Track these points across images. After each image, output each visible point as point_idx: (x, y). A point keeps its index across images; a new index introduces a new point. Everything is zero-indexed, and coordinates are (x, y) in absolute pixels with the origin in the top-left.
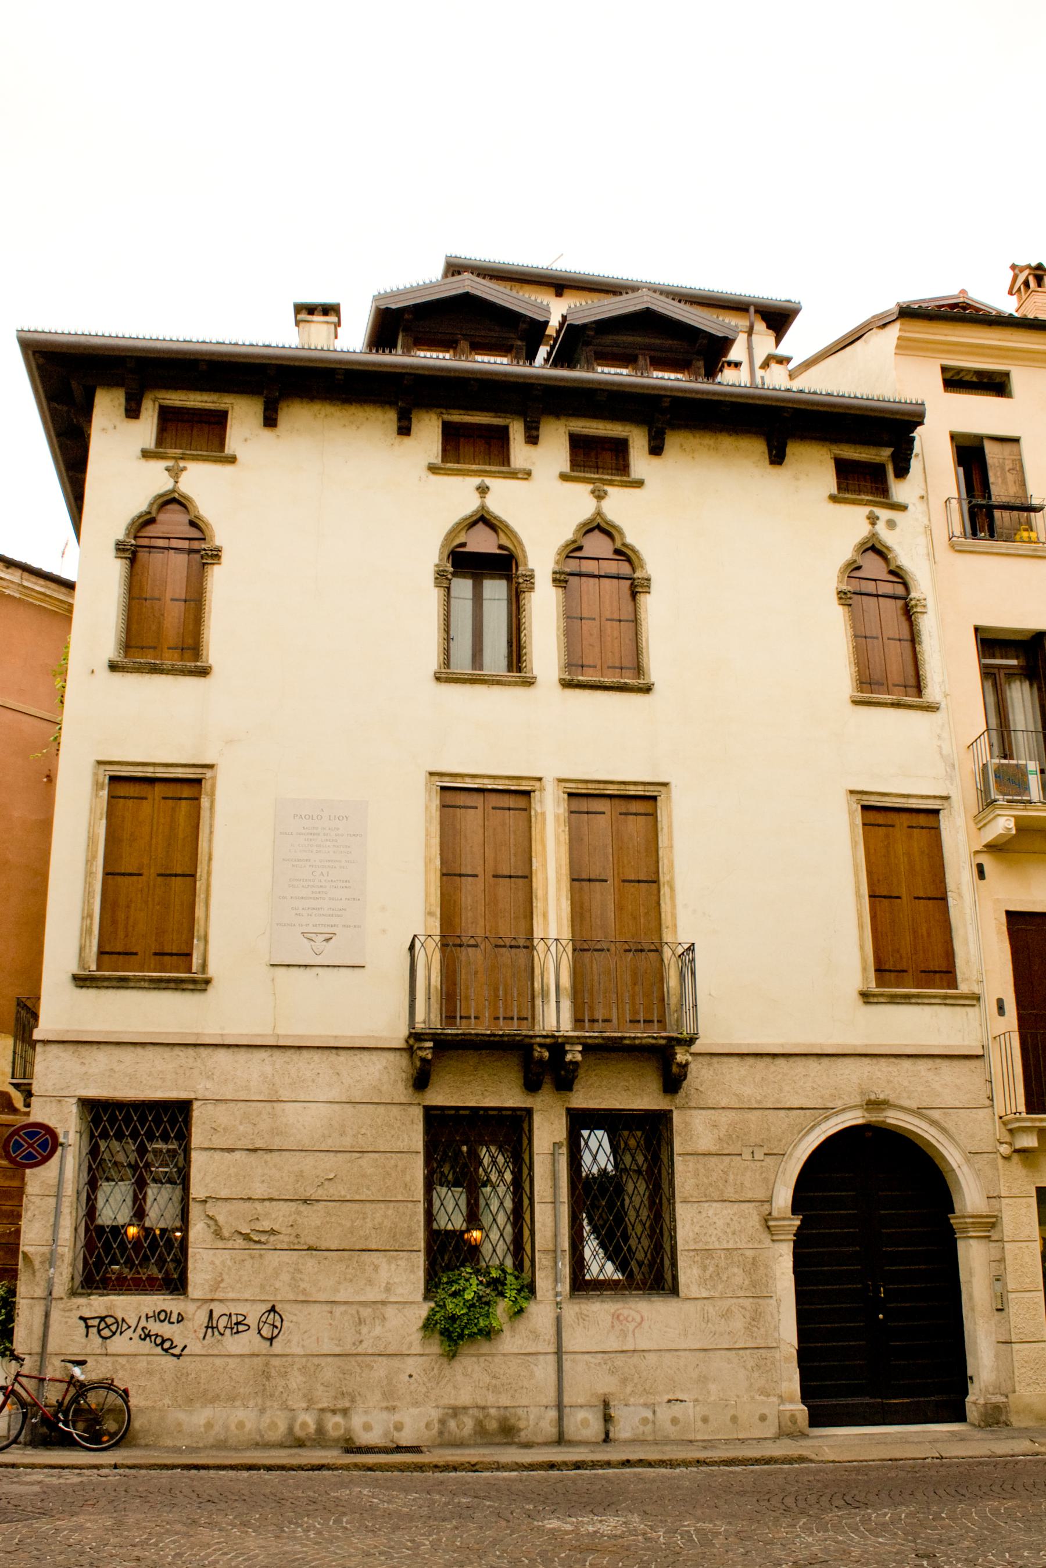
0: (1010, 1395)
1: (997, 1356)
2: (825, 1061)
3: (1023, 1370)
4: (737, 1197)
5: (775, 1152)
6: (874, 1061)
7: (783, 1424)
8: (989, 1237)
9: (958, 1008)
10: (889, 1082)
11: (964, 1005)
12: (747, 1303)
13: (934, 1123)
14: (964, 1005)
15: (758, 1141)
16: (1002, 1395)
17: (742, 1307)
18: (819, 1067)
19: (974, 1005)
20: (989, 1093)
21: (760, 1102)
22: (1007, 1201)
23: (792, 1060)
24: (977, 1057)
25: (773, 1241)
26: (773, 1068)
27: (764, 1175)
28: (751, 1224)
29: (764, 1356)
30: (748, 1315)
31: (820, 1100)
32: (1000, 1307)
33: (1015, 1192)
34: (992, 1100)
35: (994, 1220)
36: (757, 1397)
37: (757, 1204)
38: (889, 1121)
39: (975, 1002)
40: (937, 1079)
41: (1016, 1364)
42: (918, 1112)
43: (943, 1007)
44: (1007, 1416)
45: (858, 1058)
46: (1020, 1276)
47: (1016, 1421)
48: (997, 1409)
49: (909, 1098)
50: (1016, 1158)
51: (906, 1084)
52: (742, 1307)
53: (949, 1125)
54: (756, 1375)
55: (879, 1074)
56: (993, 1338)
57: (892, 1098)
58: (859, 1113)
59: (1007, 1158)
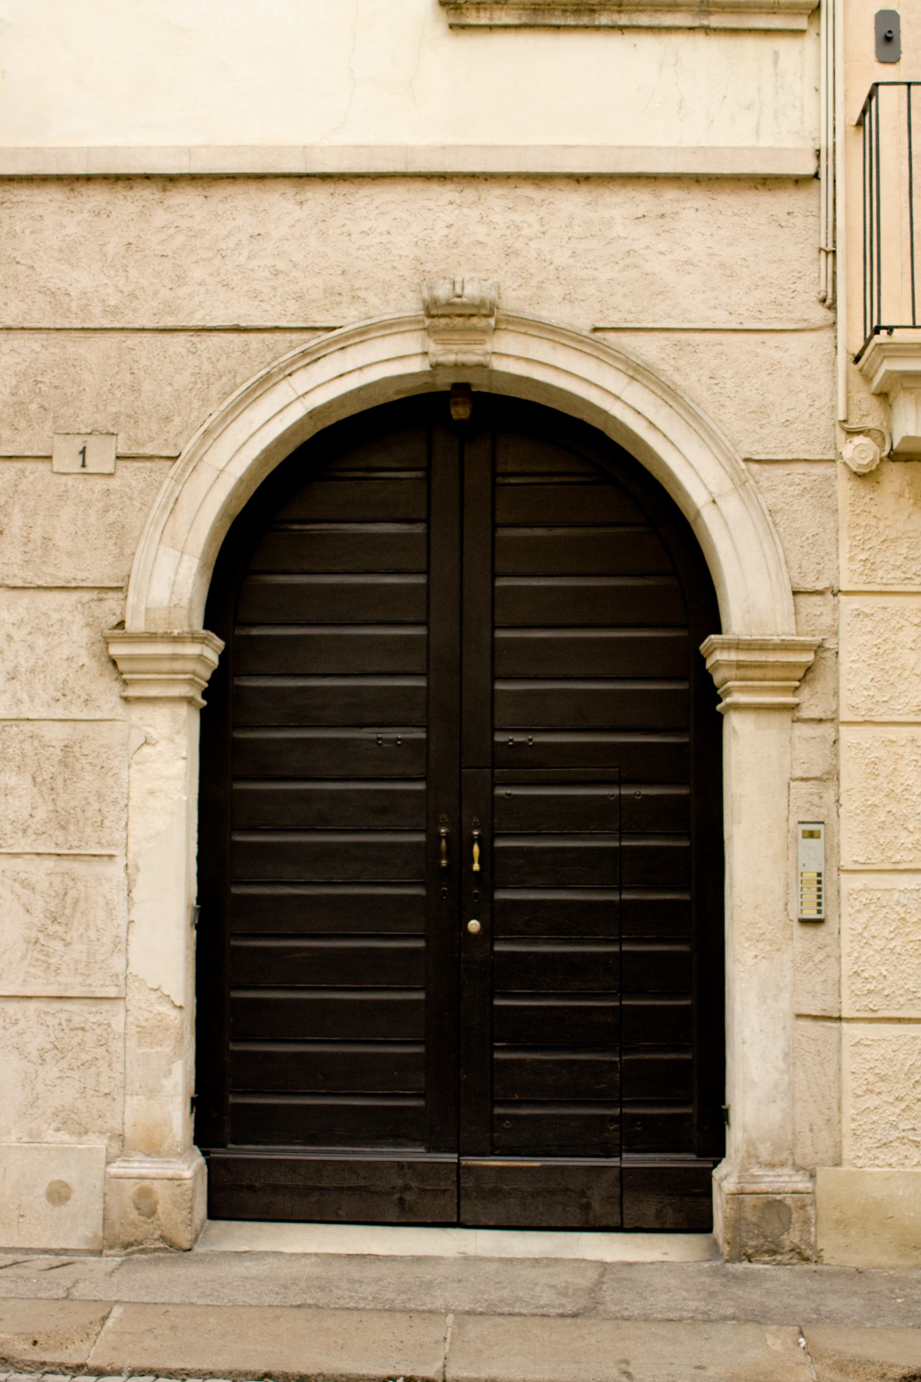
0: (821, 1173)
1: (791, 1057)
2: (319, 195)
3: (871, 1101)
4: (29, 576)
5: (148, 450)
6: (470, 193)
7: (114, 1214)
8: (795, 707)
9: (749, 44)
10: (509, 253)
11: (767, 32)
12: (40, 872)
13: (638, 372)
14: (767, 32)
15: (103, 421)
16: (798, 1168)
17: (24, 884)
18: (298, 213)
19: (799, 33)
20: (823, 287)
21: (113, 311)
22: (856, 603)
23: (219, 192)
24: (798, 181)
25: (126, 699)
26: (160, 217)
27: (111, 517)
28: (65, 651)
29: (77, 1021)
30: (39, 904)
31: (292, 306)
32: (812, 914)
33: (883, 577)
34: (833, 307)
35: (808, 657)
36: (50, 1135)
37: (87, 596)
38: (499, 365)
39: (801, 23)
40: (663, 246)
41: (849, 1083)
42: (595, 340)
43: (701, 41)
44: (805, 1230)
45: (417, 186)
46: (882, 826)
47: (835, 1249)
48: (774, 1206)
49: (567, 298)
50: (895, 475)
51: (562, 258)
52: (24, 884)
53: (691, 382)
54: (51, 1071)
55: (481, 232)
56: (785, 1005)
57: (513, 300)
58: (411, 343)
59: (865, 477)
